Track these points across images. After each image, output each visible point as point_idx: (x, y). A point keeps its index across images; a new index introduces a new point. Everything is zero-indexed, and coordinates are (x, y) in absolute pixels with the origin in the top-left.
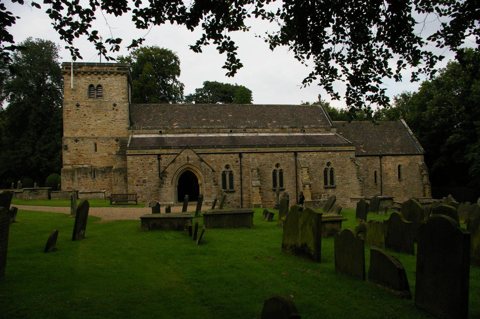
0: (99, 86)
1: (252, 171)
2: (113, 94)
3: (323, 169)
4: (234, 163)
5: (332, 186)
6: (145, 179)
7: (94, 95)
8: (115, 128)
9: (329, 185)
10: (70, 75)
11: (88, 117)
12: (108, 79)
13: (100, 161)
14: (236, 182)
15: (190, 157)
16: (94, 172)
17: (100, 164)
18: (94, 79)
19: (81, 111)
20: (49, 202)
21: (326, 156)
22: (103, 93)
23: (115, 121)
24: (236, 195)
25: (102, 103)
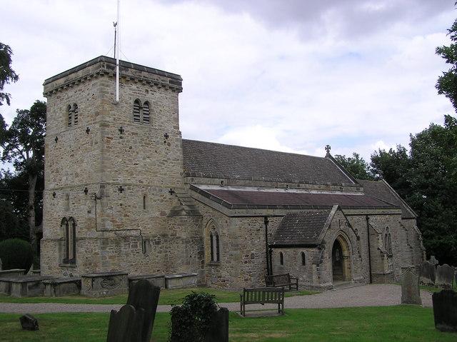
0: (147, 103)
12: (157, 95)
17: (150, 229)
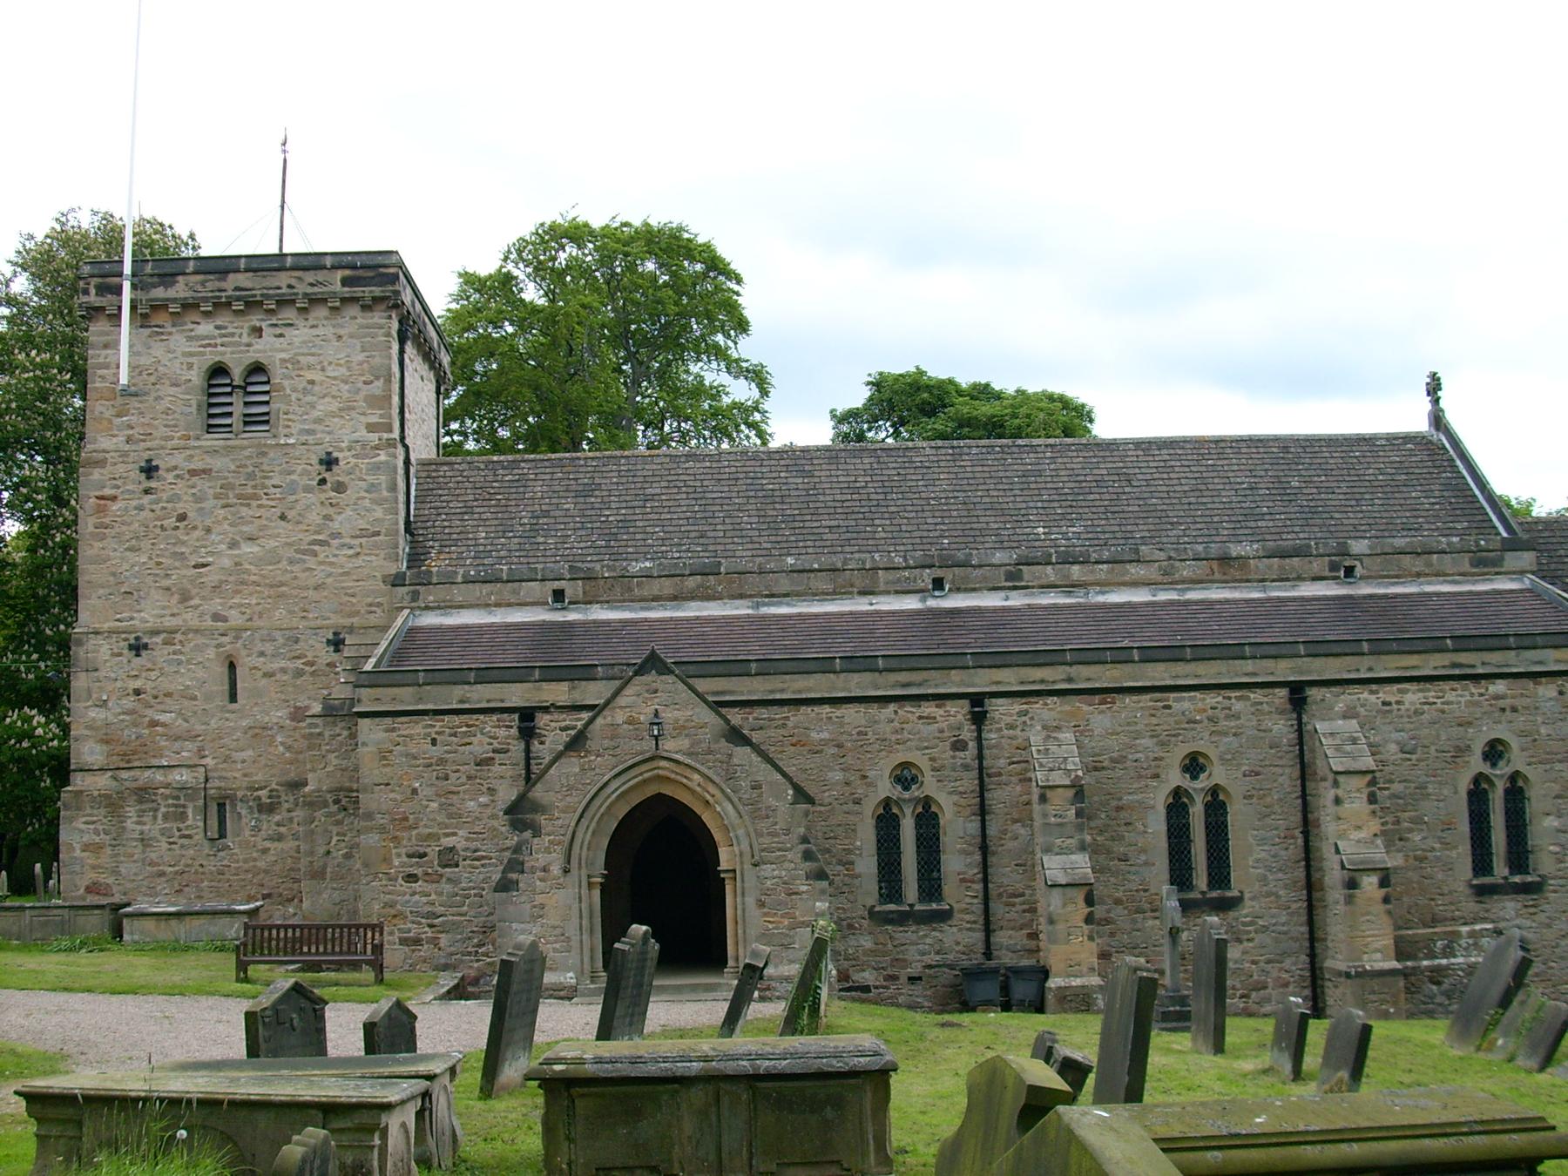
0: (257, 369)
1: (1043, 799)
2: (325, 406)
3: (1464, 783)
4: (945, 754)
5: (1517, 879)
6: (448, 842)
7: (230, 414)
8: (329, 580)
9: (1500, 870)
10: (117, 317)
11: (195, 528)
12: (301, 334)
13: (250, 753)
14: (956, 862)
15: (668, 715)
16: (221, 806)
17: (246, 768)
18: (233, 335)
19: (165, 496)
20: (113, 962)
21: (1477, 704)
22: (274, 406)
23: (329, 545)
24: (959, 937)
25: (264, 454)
